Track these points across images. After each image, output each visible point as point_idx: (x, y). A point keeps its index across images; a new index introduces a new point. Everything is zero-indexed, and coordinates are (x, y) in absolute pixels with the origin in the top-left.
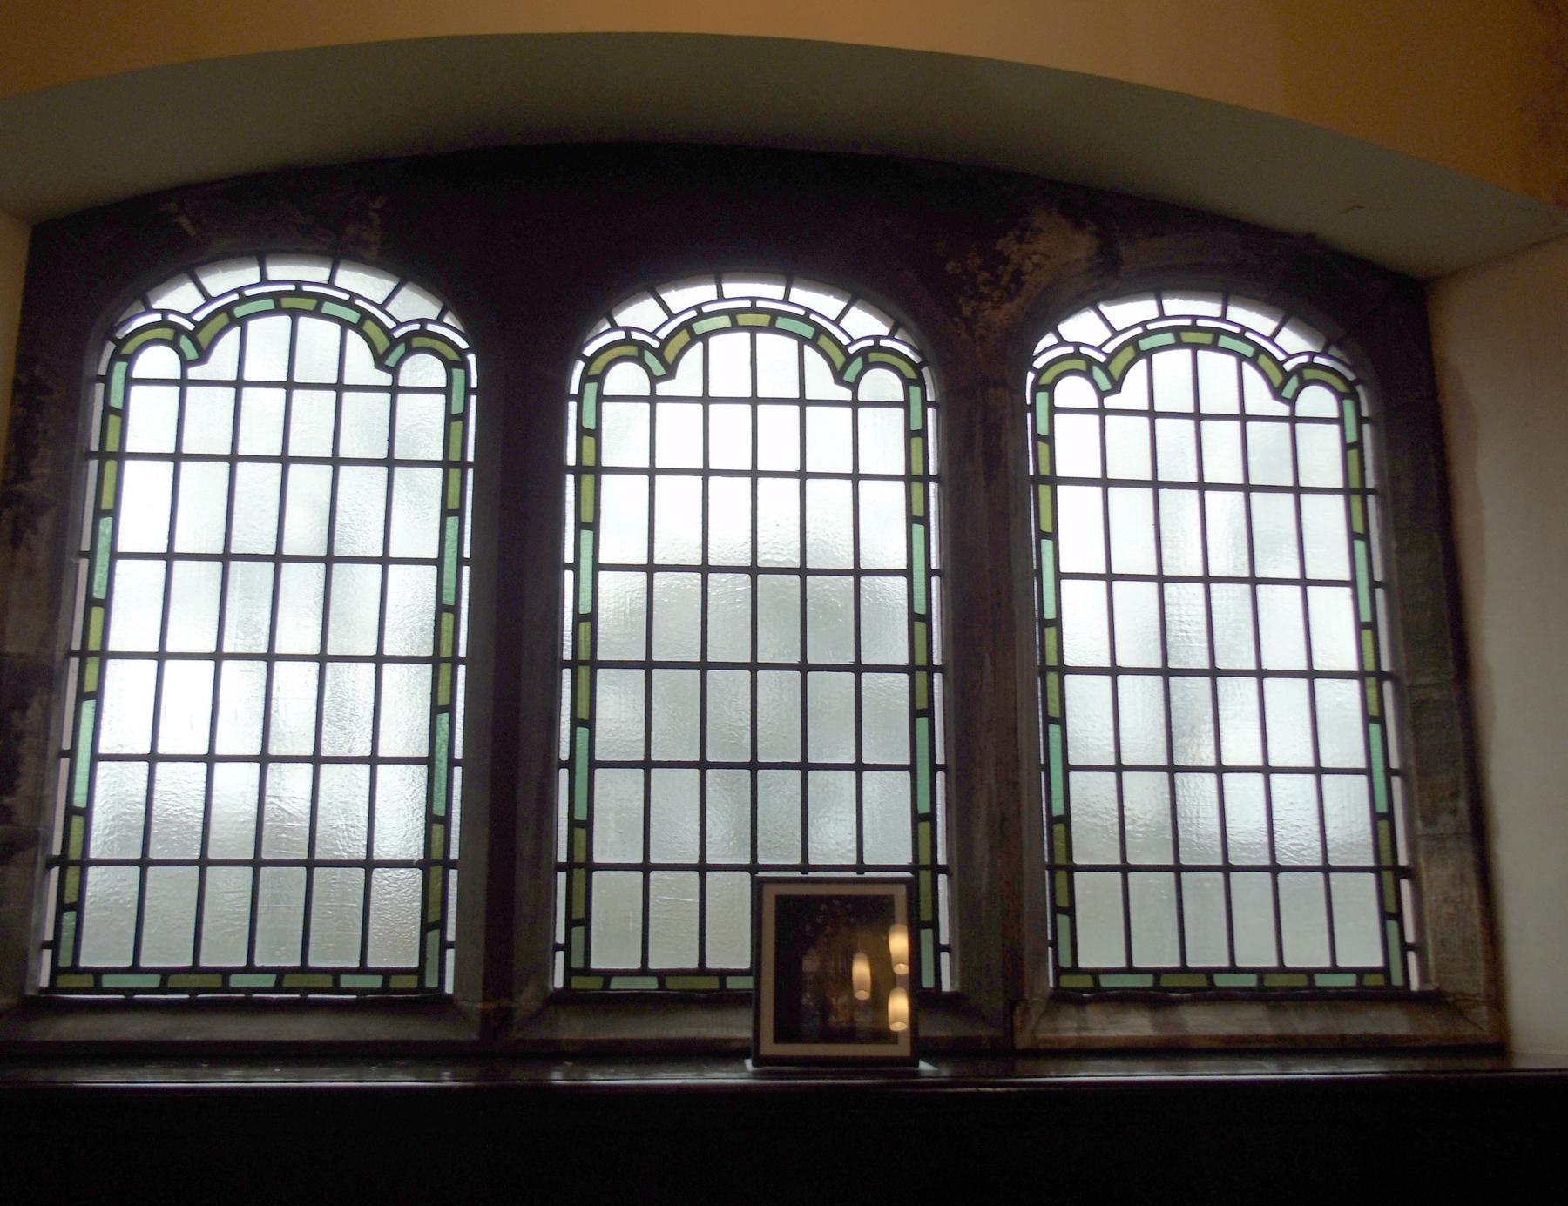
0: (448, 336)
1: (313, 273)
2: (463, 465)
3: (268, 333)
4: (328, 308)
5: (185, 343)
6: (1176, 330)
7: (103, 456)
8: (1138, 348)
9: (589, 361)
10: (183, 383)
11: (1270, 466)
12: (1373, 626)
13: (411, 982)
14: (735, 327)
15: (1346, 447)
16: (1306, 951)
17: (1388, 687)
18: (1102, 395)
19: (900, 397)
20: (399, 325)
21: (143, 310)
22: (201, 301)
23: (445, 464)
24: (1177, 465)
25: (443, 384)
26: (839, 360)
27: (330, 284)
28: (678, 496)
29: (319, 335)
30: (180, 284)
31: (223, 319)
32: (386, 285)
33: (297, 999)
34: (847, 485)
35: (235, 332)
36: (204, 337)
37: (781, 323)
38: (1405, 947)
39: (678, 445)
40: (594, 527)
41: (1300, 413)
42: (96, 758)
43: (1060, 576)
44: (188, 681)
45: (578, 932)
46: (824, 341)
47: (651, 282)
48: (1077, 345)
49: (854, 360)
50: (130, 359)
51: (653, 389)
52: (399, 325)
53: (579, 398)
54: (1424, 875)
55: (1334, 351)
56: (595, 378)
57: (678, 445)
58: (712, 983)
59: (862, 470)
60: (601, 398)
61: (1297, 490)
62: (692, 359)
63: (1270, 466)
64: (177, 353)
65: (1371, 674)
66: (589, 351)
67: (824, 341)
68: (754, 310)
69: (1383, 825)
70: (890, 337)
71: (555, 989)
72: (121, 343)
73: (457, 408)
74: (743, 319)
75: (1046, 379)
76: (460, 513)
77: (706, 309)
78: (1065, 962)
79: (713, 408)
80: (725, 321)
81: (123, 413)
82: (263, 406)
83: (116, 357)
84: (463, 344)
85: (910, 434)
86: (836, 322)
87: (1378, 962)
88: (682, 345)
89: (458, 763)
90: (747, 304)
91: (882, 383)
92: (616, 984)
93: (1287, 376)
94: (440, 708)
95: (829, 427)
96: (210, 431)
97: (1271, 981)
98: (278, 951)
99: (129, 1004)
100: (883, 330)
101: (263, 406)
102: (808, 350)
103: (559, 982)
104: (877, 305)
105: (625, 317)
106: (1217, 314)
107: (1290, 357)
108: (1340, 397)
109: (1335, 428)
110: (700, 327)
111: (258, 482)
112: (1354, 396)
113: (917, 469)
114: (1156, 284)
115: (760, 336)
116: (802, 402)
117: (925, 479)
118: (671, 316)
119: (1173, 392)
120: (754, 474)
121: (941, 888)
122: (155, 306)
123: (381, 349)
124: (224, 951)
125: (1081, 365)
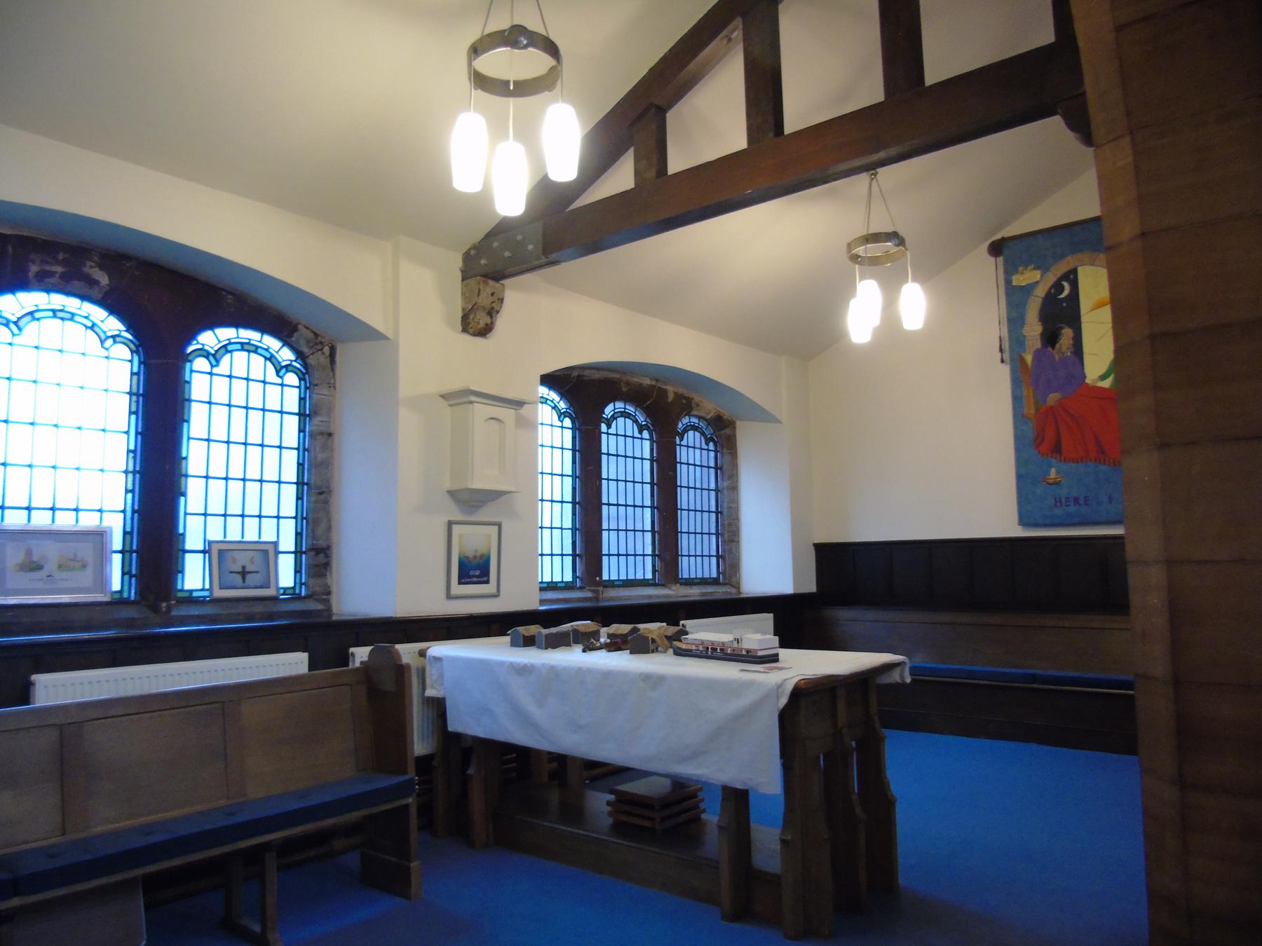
6: (242, 344)
7: (137, 395)
8: (226, 348)
11: (273, 403)
14: (242, 349)
22: (218, 342)
24: (255, 402)
29: (257, 360)
38: (301, 584)
39: (220, 395)
41: (285, 383)
42: (186, 514)
43: (189, 438)
47: (211, 326)
48: (203, 345)
54: (727, 557)
57: (220, 395)
58: (554, 585)
61: (562, 448)
62: (226, 360)
63: (273, 403)
67: (556, 408)
70: (295, 361)
80: (239, 347)
90: (247, 341)
92: (195, 594)
93: (561, 413)
95: (273, 392)
97: (550, 585)
100: (122, 328)
106: (623, 407)
107: (284, 361)
108: (132, 352)
110: (230, 348)
118: (220, 342)
119: (240, 370)
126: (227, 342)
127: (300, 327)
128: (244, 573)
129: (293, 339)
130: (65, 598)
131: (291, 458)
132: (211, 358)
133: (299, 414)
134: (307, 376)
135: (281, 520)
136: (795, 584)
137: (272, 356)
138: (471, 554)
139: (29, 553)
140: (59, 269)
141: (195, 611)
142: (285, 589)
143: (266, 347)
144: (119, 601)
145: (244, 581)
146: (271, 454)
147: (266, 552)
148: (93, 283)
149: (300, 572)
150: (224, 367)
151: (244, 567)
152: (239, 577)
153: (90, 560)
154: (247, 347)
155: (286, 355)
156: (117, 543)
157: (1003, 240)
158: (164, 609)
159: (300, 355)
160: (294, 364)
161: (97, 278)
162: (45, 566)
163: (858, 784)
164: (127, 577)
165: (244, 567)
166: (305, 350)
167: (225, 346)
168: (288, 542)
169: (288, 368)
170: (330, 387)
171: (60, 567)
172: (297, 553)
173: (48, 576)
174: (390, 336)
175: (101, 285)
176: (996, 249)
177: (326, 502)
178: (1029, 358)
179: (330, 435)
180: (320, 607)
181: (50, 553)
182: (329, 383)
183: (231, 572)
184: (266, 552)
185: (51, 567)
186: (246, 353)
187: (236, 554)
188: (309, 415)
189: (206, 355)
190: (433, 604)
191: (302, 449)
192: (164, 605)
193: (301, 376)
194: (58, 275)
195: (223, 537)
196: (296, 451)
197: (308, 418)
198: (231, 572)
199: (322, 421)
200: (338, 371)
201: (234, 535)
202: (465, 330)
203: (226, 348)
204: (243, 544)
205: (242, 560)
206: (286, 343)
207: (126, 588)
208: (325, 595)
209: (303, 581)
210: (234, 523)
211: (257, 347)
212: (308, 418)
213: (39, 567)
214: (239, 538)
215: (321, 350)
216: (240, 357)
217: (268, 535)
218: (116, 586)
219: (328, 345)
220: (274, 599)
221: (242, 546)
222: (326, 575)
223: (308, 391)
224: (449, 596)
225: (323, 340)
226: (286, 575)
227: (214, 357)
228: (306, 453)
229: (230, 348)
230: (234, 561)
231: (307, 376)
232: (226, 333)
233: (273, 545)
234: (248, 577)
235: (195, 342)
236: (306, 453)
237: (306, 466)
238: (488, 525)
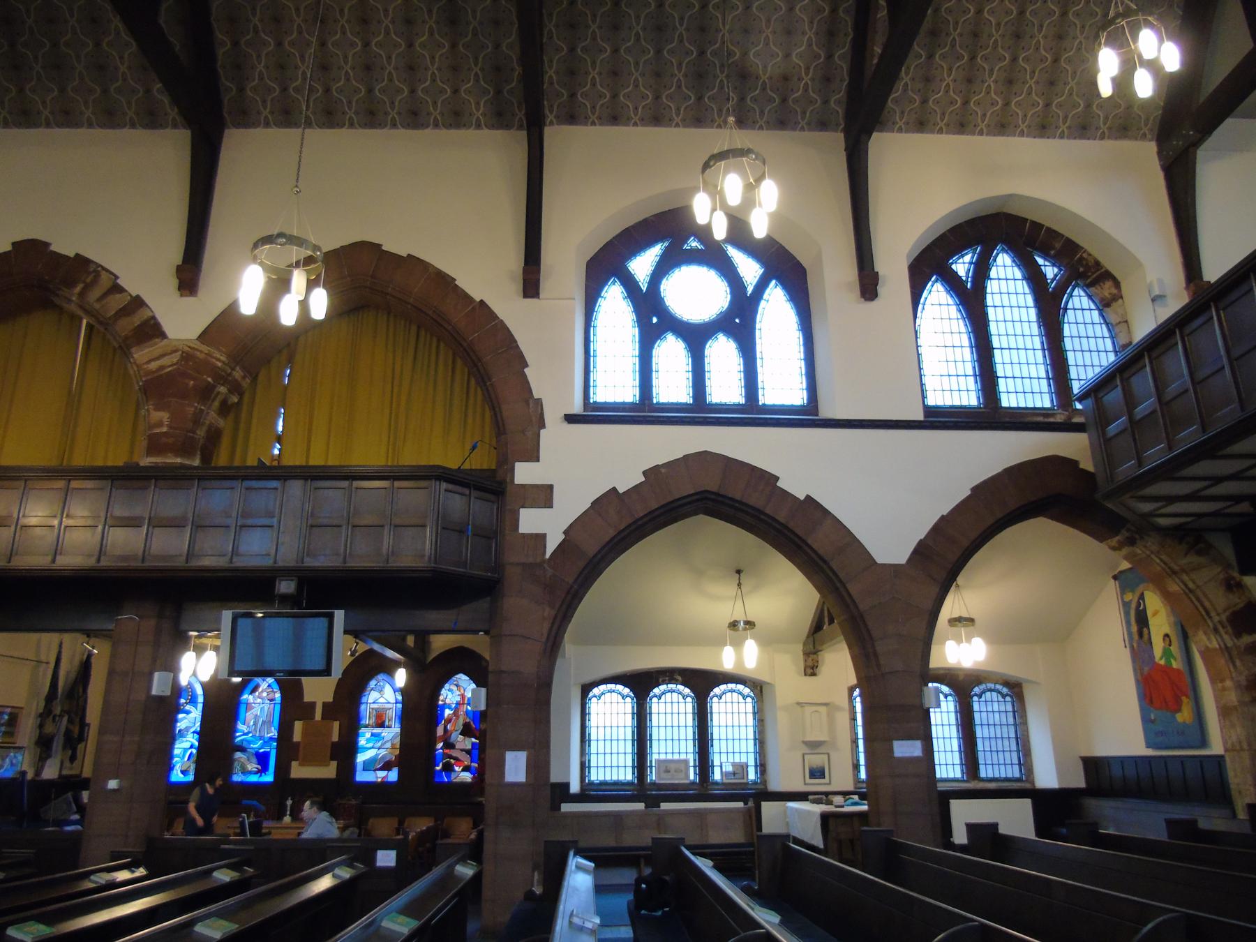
8: (664, 693)
11: (1002, 708)
16: (622, 778)
47: (658, 685)
56: (651, 699)
62: (724, 696)
91: (1008, 699)
130: (676, 782)
136: (1059, 783)
138: (815, 767)
141: (716, 787)
144: (693, 783)
147: (742, 766)
150: (983, 699)
153: (683, 769)
156: (692, 764)
157: (1121, 572)
163: (858, 874)
168: (752, 762)
169: (1007, 695)
172: (756, 766)
176: (1115, 578)
178: (1135, 645)
181: (672, 766)
184: (742, 766)
185: (672, 771)
189: (976, 695)
190: (798, 786)
191: (754, 726)
202: (805, 675)
203: (664, 693)
208: (764, 782)
210: (737, 756)
217: (744, 760)
218: (692, 777)
220: (747, 784)
224: (805, 784)
226: (752, 776)
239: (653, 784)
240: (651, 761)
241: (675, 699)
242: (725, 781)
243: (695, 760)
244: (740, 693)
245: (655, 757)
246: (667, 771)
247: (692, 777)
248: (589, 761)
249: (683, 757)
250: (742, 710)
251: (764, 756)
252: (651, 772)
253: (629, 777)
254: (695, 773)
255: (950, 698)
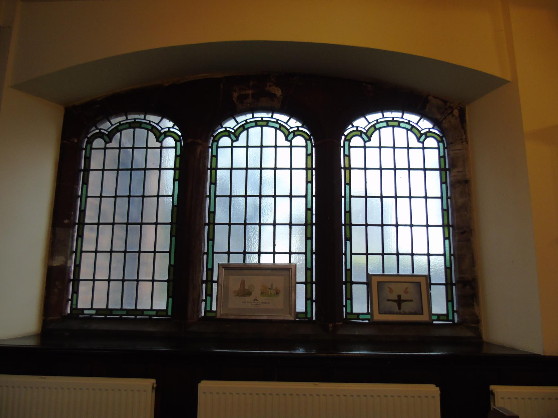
0: (175, 131)
1: (397, 115)
2: (312, 169)
3: (255, 132)
4: (402, 125)
5: (232, 136)
8: (375, 128)
9: (346, 136)
10: (365, 147)
12: (447, 210)
13: (304, 316)
14: (388, 126)
15: (440, 157)
16: (144, 304)
17: (451, 228)
18: (365, 142)
19: (437, 146)
20: (291, 128)
21: (221, 127)
22: (236, 124)
23: (307, 169)
25: (174, 146)
26: (419, 135)
27: (145, 119)
28: (373, 175)
29: (400, 133)
30: (230, 120)
31: (241, 129)
32: (418, 118)
33: (133, 318)
34: (379, 171)
35: (245, 132)
36: (237, 134)
37: (270, 124)
38: (453, 311)
39: (373, 160)
40: (350, 184)
44: (106, 231)
45: (349, 302)
46: (414, 130)
47: (363, 114)
48: (357, 127)
49: (423, 135)
50: (217, 142)
51: (365, 144)
52: (291, 128)
53: (344, 147)
55: (176, 127)
56: (90, 142)
57: (373, 160)
59: (293, 167)
60: (218, 147)
62: (244, 134)
64: (102, 139)
65: (446, 226)
66: (346, 133)
68: (262, 120)
69: (448, 270)
70: (433, 128)
71: (68, 313)
72: (214, 137)
73: (309, 152)
74: (390, 123)
75: (348, 138)
76: (311, 182)
77: (379, 121)
78: (349, 311)
79: (274, 149)
80: (385, 124)
81: (216, 157)
82: (387, 154)
83: (213, 141)
84: (180, 134)
85: (307, 155)
86: (286, 123)
87: (445, 312)
88: (372, 132)
89: (344, 254)
90: (260, 119)
91: (299, 141)
94: (308, 238)
95: (283, 154)
96: (373, 162)
98: (100, 304)
99: (121, 320)
100: (431, 126)
101: (387, 154)
102: (409, 132)
103: (203, 314)
104: (298, 119)
105: (356, 123)
109: (437, 151)
110: (378, 126)
111: (388, 175)
112: (310, 140)
113: (309, 166)
114: (382, 109)
115: (395, 128)
116: (408, 148)
117: (312, 169)
118: (369, 123)
120: (395, 169)
121: (214, 287)
122: (224, 126)
123: (158, 136)
124: (114, 305)
125: (359, 133)
126: (375, 122)
127: (430, 98)
128: (399, 301)
129: (427, 110)
131: (436, 207)
132: (364, 136)
133: (440, 169)
134: (444, 139)
135: (276, 251)
137: (413, 127)
139: (243, 283)
140: (250, 92)
142: (439, 315)
143: (407, 121)
145: (400, 308)
146: (374, 190)
148: (272, 96)
149: (452, 301)
150: (374, 141)
151: (399, 296)
152: (395, 305)
154: (393, 124)
155: (425, 125)
156: (301, 276)
158: (330, 329)
159: (436, 123)
160: (432, 130)
161: (274, 92)
162: (252, 293)
164: (309, 302)
165: (399, 296)
166: (438, 117)
167: (374, 126)
170: (463, 142)
171: (262, 293)
172: (448, 284)
173: (255, 300)
174: (508, 77)
175: (277, 96)
177: (469, 240)
179: (467, 182)
180: (469, 334)
181: (254, 281)
182: (462, 139)
183: (388, 300)
185: (256, 293)
186: (391, 128)
187: (392, 286)
188: (448, 170)
192: (331, 325)
193: (439, 139)
194: (250, 96)
195: (396, 272)
196: (440, 200)
197: (448, 172)
198: (388, 300)
199: (458, 172)
200: (468, 129)
201: (391, 270)
203: (375, 128)
204: (415, 278)
205: (398, 290)
206: (423, 115)
207: (309, 309)
209: (455, 309)
211: (399, 122)
212: (448, 172)
213: (249, 294)
214: (395, 273)
215: (452, 112)
216: (387, 132)
218: (301, 307)
219: (456, 108)
220: (429, 325)
221: (398, 278)
222: (473, 305)
223: (446, 150)
225: (452, 105)
227: (367, 135)
228: (449, 200)
229: (378, 126)
230: (391, 291)
231: (444, 139)
232: (373, 117)
233: (424, 278)
234: (403, 304)
235: (350, 126)
236: (449, 200)
237: (450, 212)
238: (107, 298)
239: (210, 318)
240: (210, 271)
241: (401, 141)
242: (378, 317)
243: (308, 270)
244: (412, 129)
245: (220, 260)
246: (245, 293)
247: (301, 307)
248: (78, 267)
249: (282, 260)
250: (283, 160)
251: (473, 263)
252: (209, 294)
253: (161, 303)
254: (308, 298)
255: (170, 142)
